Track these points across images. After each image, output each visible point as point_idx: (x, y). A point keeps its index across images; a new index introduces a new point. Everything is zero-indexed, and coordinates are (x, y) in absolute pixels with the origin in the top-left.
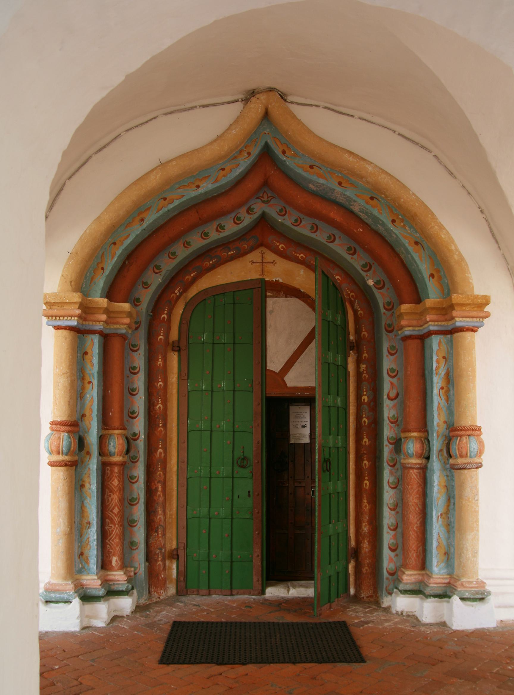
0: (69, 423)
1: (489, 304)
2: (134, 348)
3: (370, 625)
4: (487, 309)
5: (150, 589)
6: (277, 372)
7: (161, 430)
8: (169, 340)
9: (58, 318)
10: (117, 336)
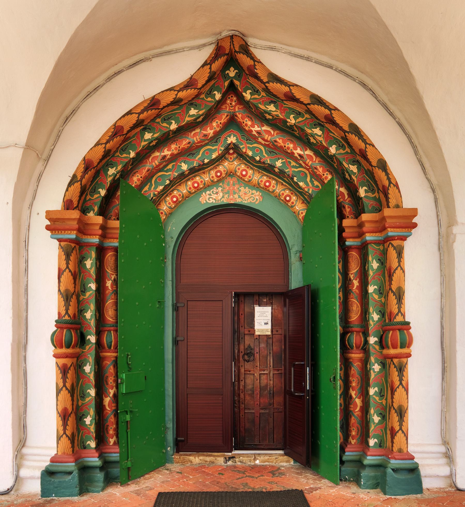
0: (71, 322)
1: (416, 216)
2: (290, 163)
3: (318, 491)
4: (415, 220)
5: (239, 410)
6: (60, 209)
7: (293, 117)
8: (164, 389)
9: (57, 232)
10: (233, 45)
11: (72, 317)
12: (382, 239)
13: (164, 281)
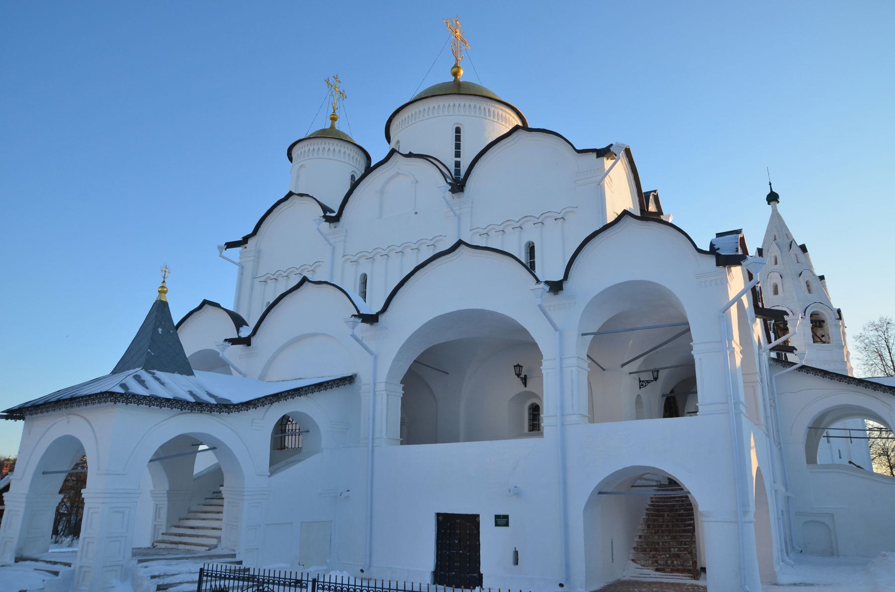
11: (744, 403)
12: (758, 320)
13: (155, 330)
